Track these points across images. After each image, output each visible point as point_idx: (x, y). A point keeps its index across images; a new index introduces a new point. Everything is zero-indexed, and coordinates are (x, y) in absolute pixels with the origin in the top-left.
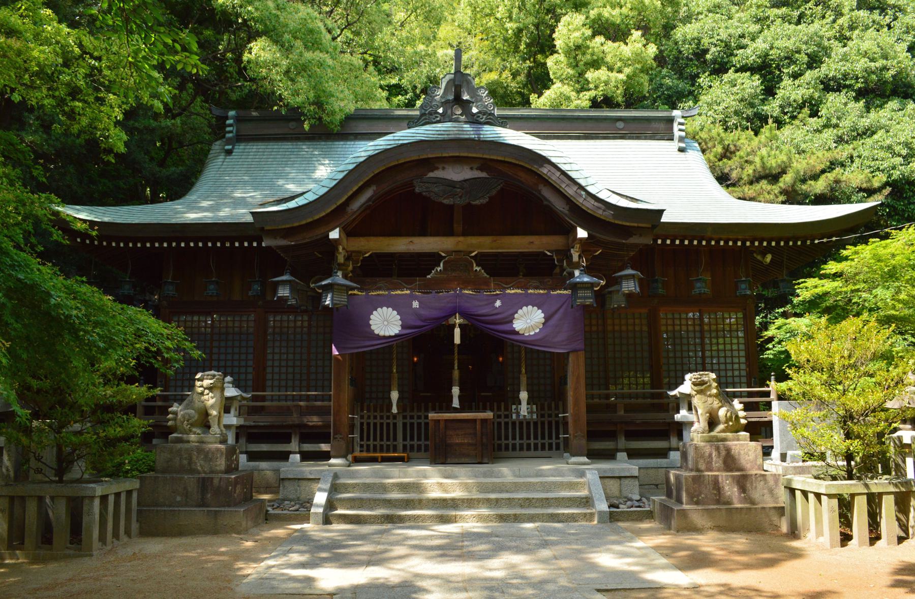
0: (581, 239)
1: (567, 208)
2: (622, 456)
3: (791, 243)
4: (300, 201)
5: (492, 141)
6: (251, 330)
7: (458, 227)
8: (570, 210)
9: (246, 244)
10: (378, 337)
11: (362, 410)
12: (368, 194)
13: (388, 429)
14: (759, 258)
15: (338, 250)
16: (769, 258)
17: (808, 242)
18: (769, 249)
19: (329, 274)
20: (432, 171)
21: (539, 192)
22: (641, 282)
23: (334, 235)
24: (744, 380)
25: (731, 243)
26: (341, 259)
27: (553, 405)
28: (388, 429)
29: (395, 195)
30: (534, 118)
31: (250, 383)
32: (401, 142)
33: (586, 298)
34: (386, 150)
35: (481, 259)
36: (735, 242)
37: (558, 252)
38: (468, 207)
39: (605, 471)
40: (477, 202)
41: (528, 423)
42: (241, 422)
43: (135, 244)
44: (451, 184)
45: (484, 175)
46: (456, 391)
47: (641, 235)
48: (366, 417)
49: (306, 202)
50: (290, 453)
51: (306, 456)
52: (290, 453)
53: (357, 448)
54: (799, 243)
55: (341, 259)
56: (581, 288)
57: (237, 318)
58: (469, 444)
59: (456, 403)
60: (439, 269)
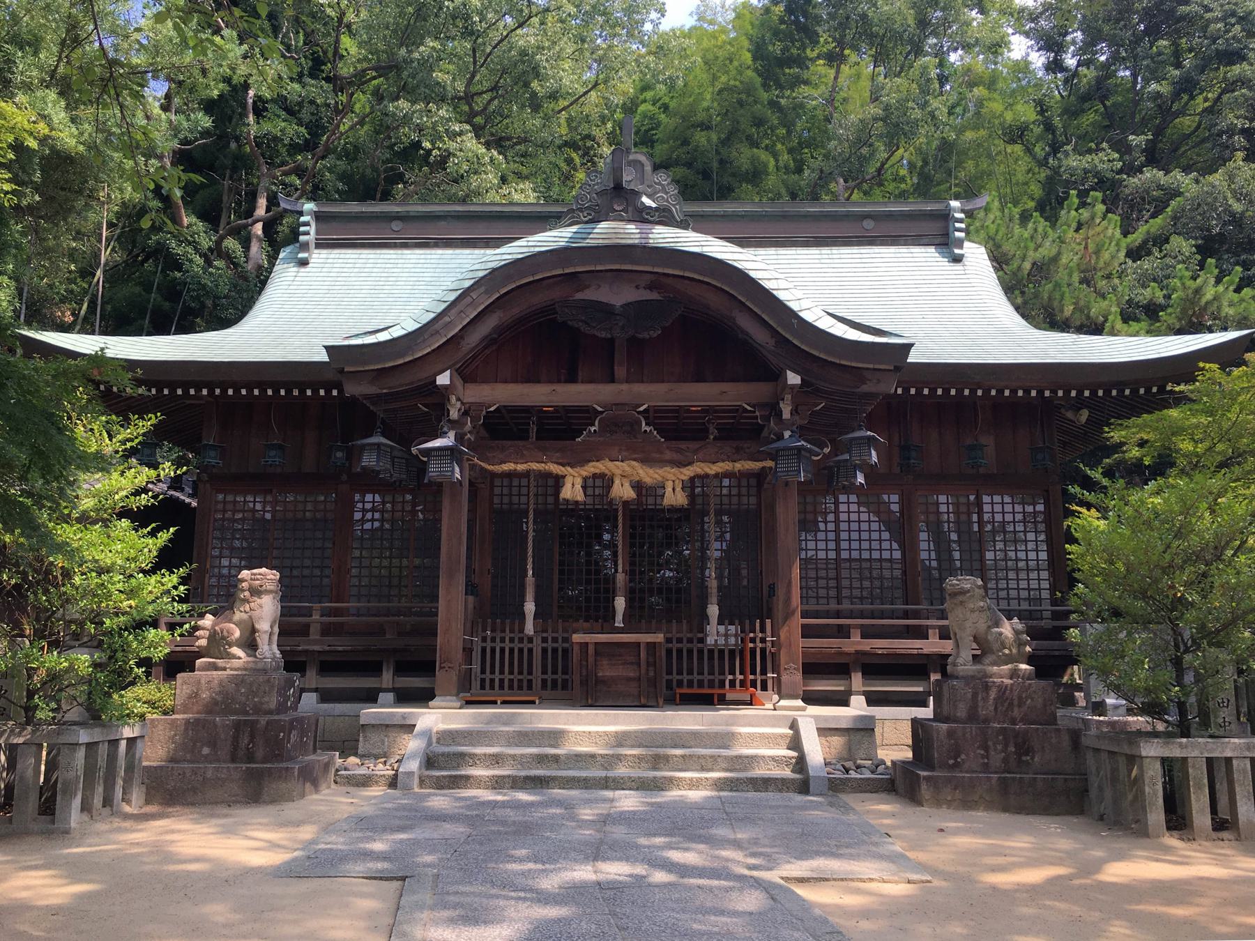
0: (793, 386)
1: (772, 342)
3: (1114, 393)
4: (383, 337)
7: (620, 371)
11: (484, 630)
13: (493, 657)
14: (1069, 415)
16: (1084, 415)
20: (582, 290)
23: (443, 379)
24: (898, 593)
27: (758, 625)
28: (493, 657)
30: (743, 216)
32: (538, 249)
35: (653, 415)
37: (762, 406)
39: (826, 719)
41: (721, 652)
43: (250, 391)
48: (498, 640)
49: (389, 337)
53: (476, 684)
54: (1127, 392)
55: (454, 414)
57: (389, 498)
58: (629, 679)
59: (619, 623)
60: (593, 429)
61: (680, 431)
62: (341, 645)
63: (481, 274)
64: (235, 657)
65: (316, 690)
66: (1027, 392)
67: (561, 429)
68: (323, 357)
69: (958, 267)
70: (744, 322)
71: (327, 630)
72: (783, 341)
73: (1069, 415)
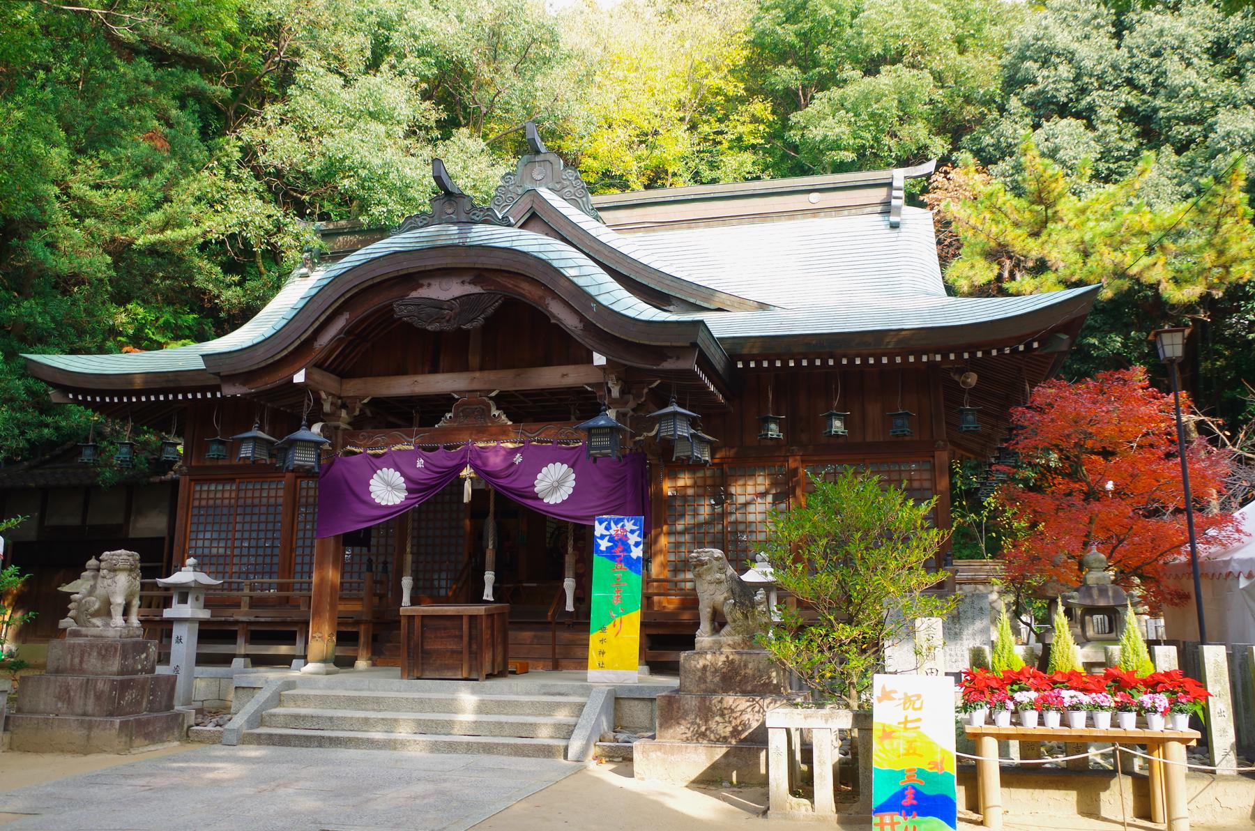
1: (580, 326)
2: (238, 663)
3: (966, 356)
5: (480, 246)
6: (280, 501)
7: (474, 360)
9: (209, 395)
10: (379, 506)
12: (340, 323)
14: (956, 378)
17: (1007, 351)
18: (973, 364)
19: (249, 430)
21: (547, 305)
23: (299, 378)
29: (377, 326)
31: (275, 568)
34: (355, 267)
35: (503, 400)
42: (205, 614)
44: (438, 304)
46: (489, 577)
47: (678, 358)
50: (234, 656)
51: (258, 661)
52: (234, 656)
62: (266, 616)
64: (94, 626)
65: (246, 656)
68: (201, 365)
69: (894, 233)
70: (557, 310)
71: (255, 603)
72: (589, 327)
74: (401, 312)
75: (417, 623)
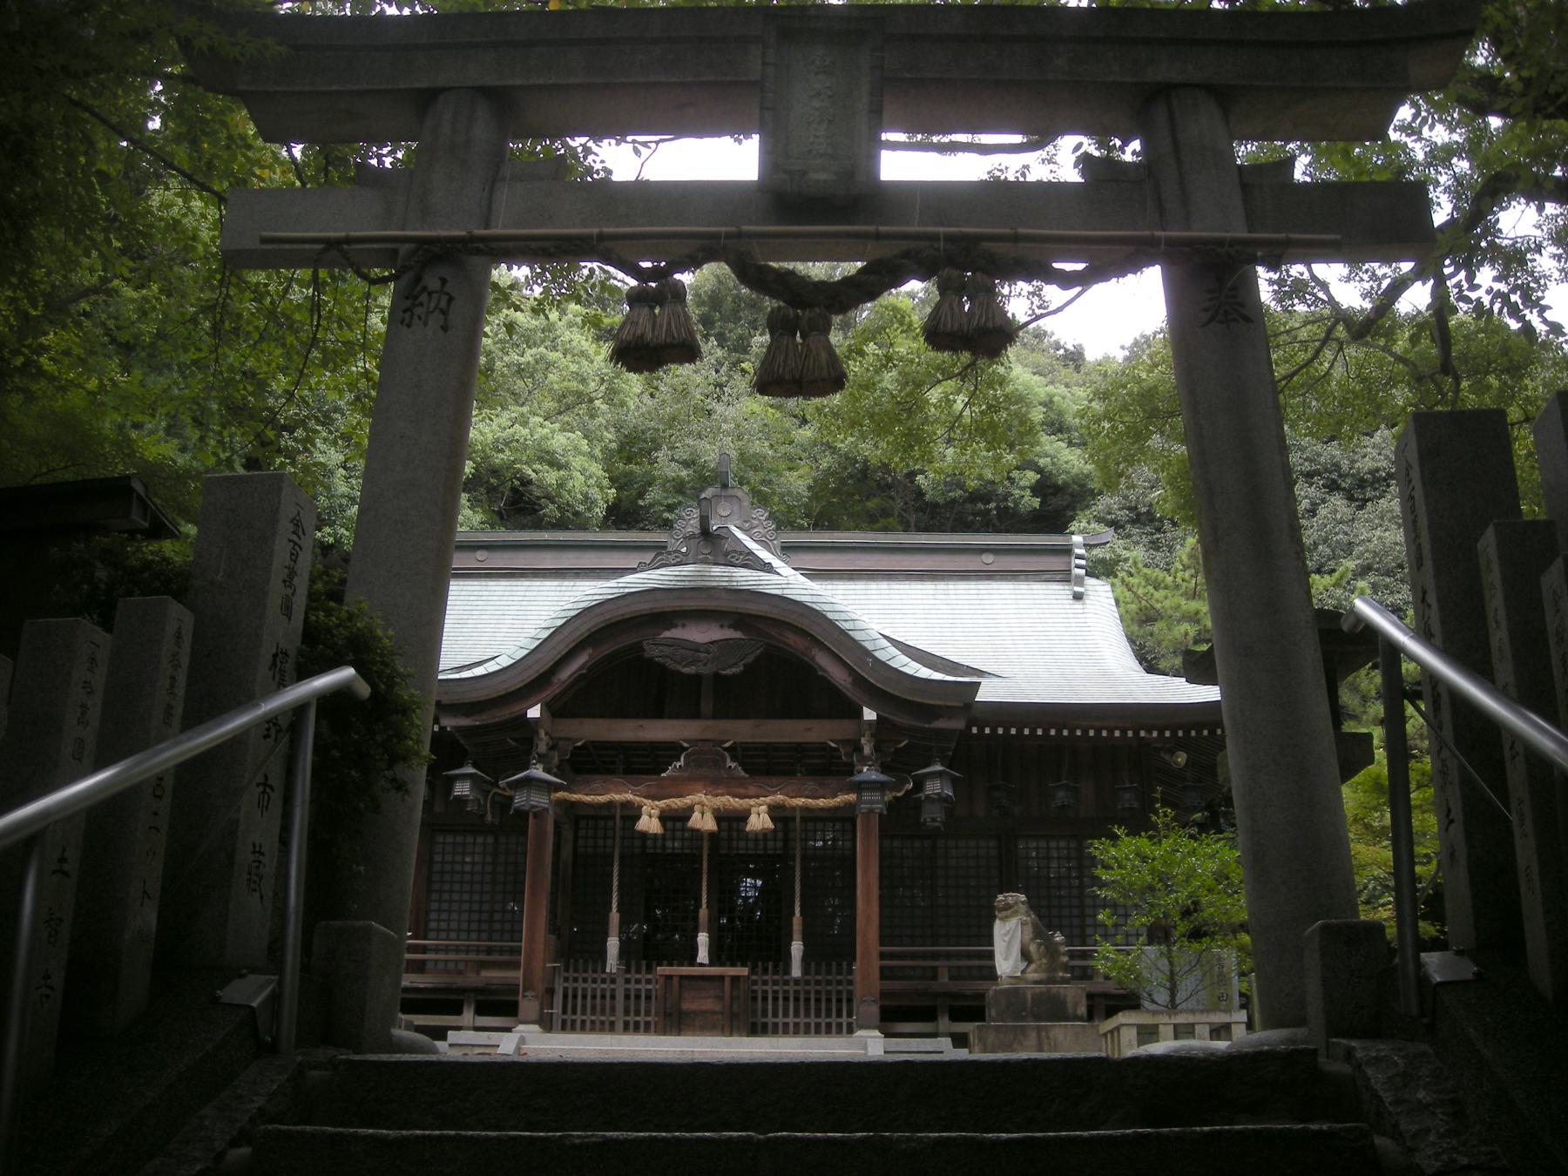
1: (850, 680)
4: (492, 667)
7: (706, 706)
8: (854, 683)
12: (582, 659)
14: (1167, 757)
15: (537, 733)
16: (1181, 758)
21: (813, 659)
22: (955, 782)
23: (534, 712)
25: (1104, 733)
26: (542, 748)
33: (871, 802)
35: (742, 753)
36: (1111, 732)
37: (844, 742)
38: (716, 676)
40: (728, 672)
45: (738, 635)
54: (1205, 733)
55: (542, 748)
56: (868, 789)
59: (703, 955)
61: (764, 764)
63: (573, 613)
66: (1124, 732)
67: (644, 763)
69: (1078, 605)
70: (822, 660)
72: (859, 681)
73: (1167, 757)
74: (653, 652)
75: (676, 981)
